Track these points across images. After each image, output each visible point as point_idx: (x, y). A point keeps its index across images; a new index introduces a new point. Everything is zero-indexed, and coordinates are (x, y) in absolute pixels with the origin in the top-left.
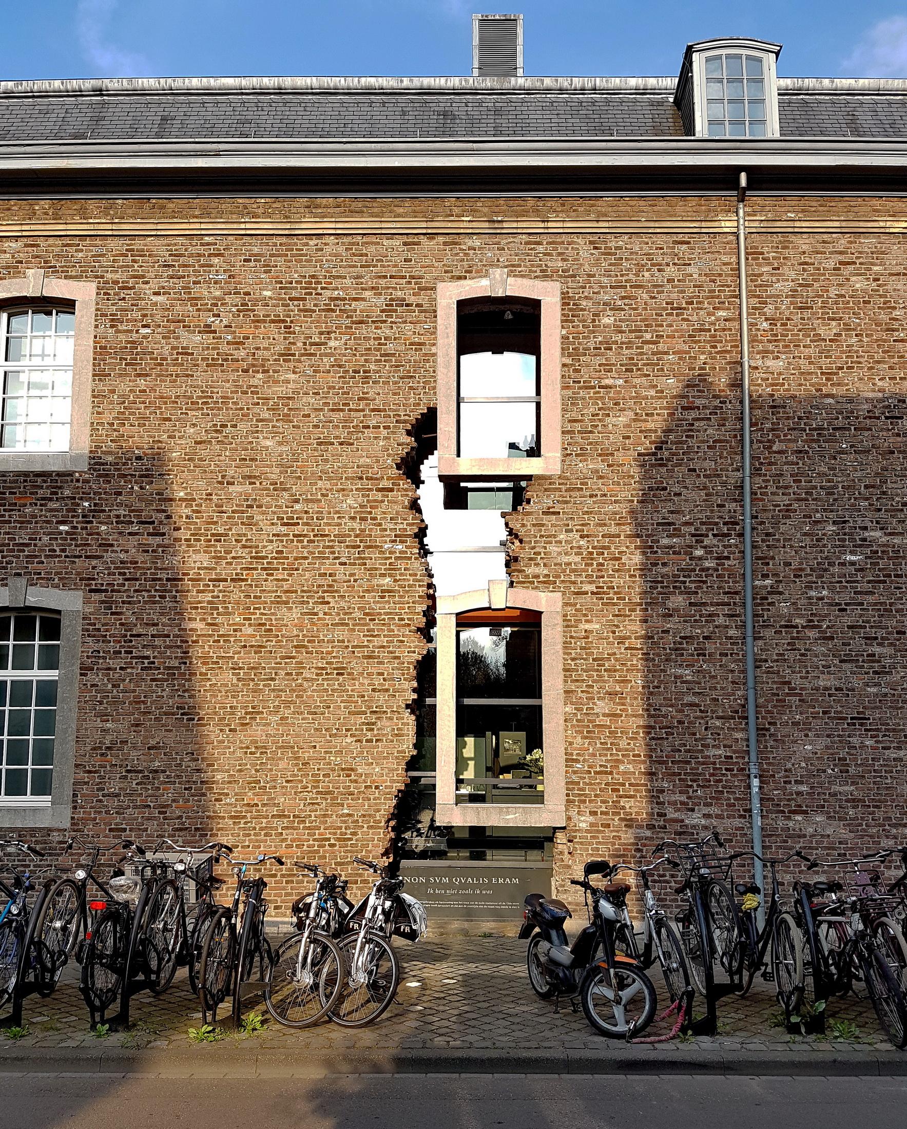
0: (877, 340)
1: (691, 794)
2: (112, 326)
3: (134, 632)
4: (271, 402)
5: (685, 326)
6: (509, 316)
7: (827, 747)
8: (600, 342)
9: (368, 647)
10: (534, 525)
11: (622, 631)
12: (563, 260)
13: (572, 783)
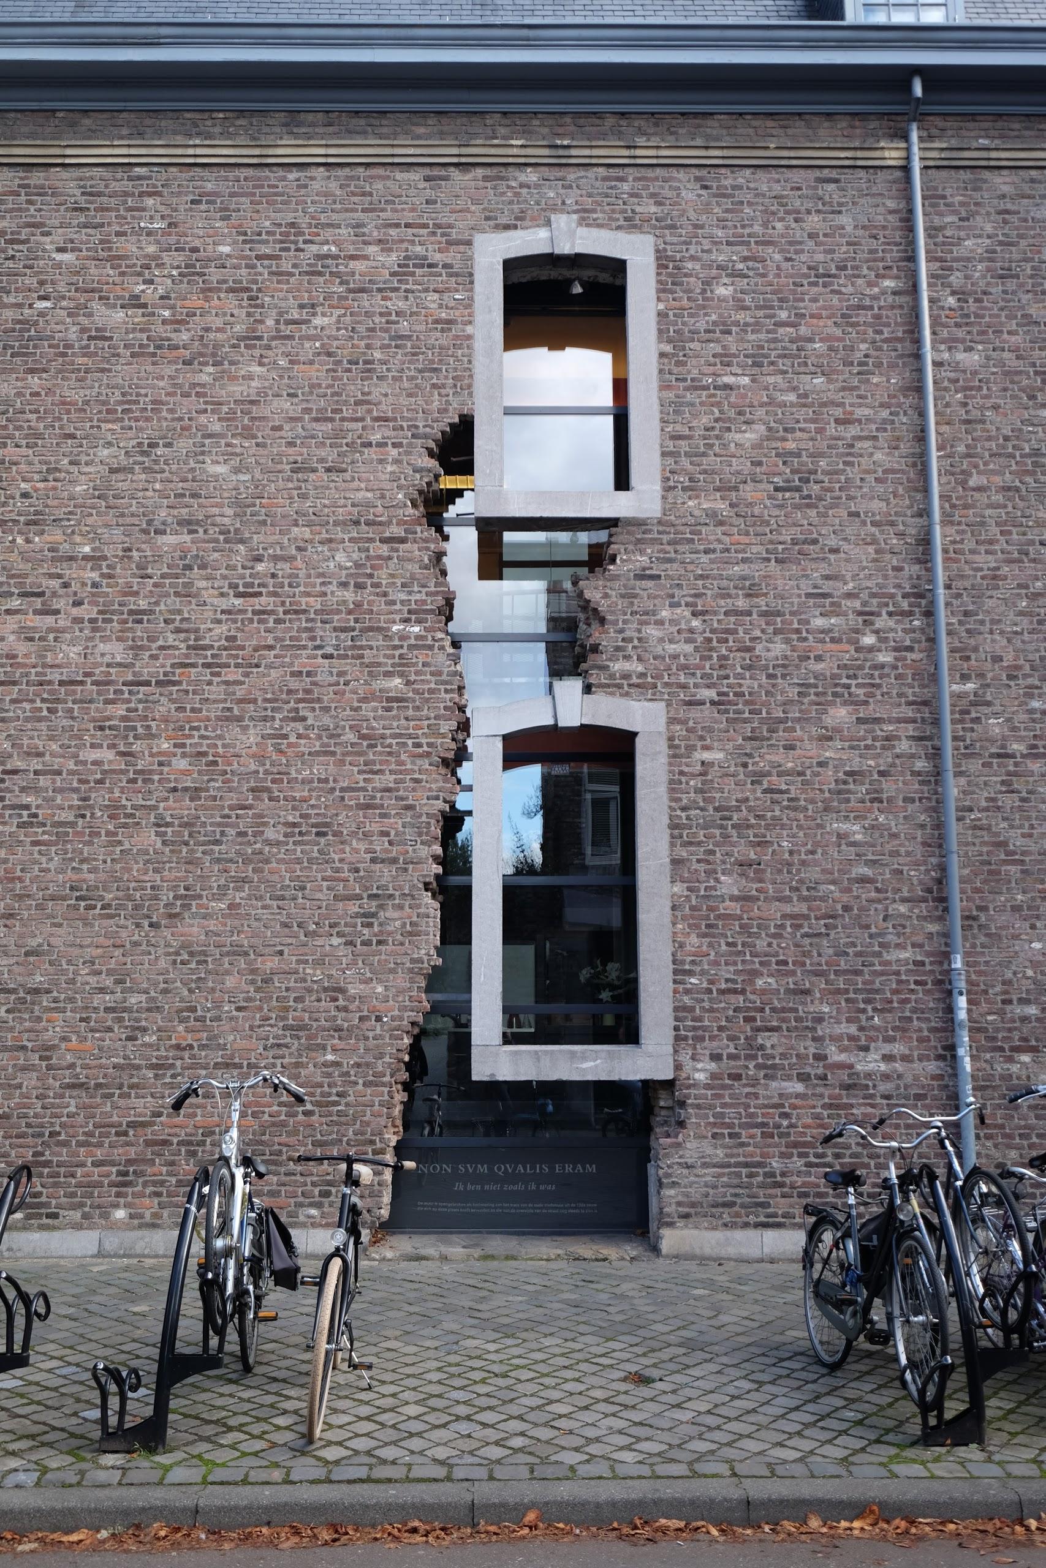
1: (864, 1023)
4: (225, 409)
9: (364, 789)
10: (623, 596)
11: (757, 763)
12: (659, 204)
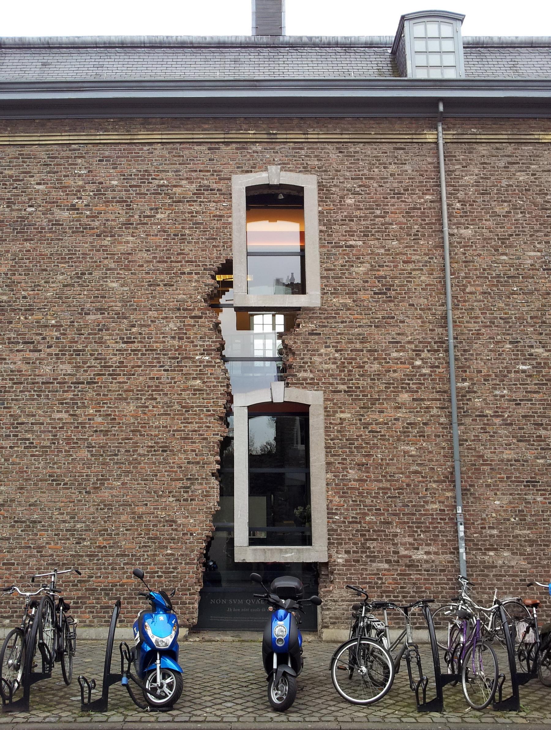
0: (535, 217)
1: (416, 537)
2: (8, 207)
3: (19, 421)
4: (116, 257)
5: (403, 206)
6: (281, 197)
7: (510, 503)
8: (345, 216)
9: (184, 431)
10: (303, 343)
13: (333, 530)
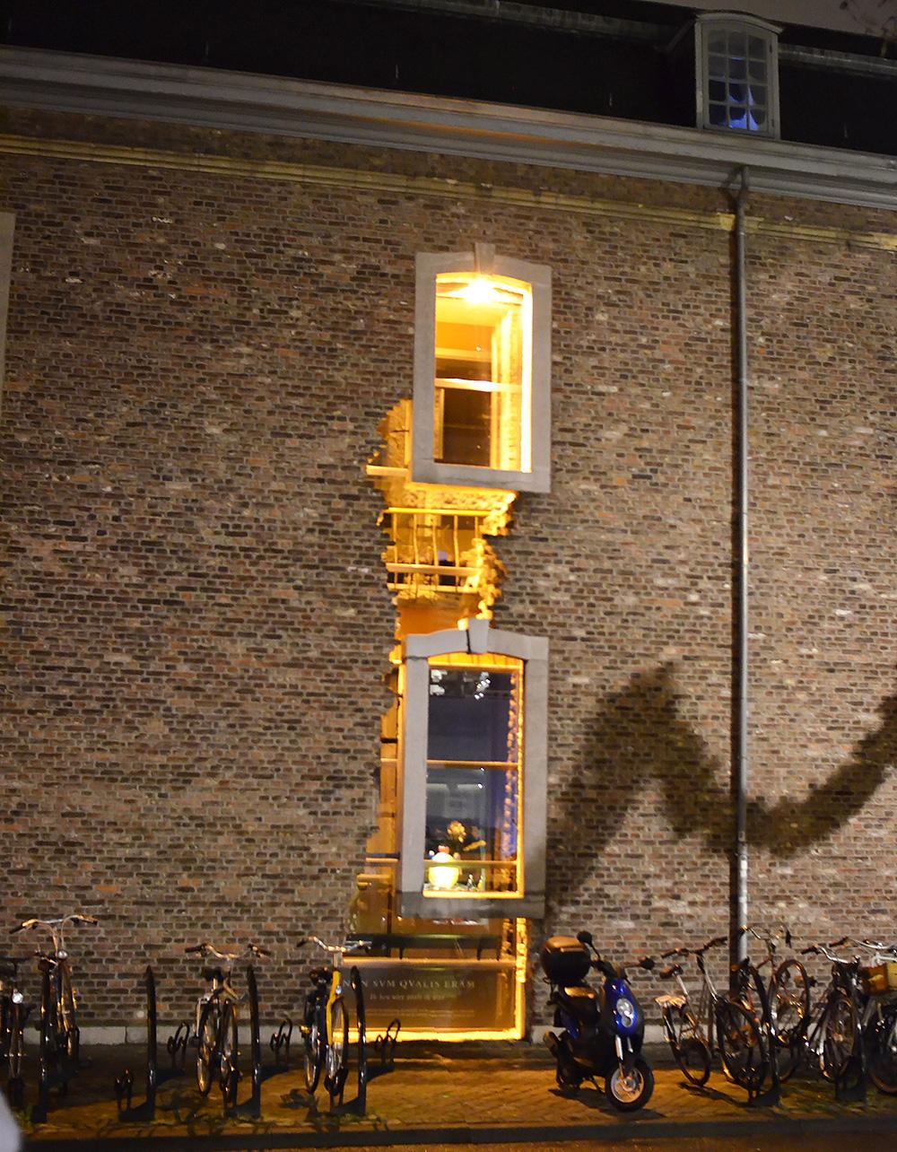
5: (681, 333)
12: (555, 241)
